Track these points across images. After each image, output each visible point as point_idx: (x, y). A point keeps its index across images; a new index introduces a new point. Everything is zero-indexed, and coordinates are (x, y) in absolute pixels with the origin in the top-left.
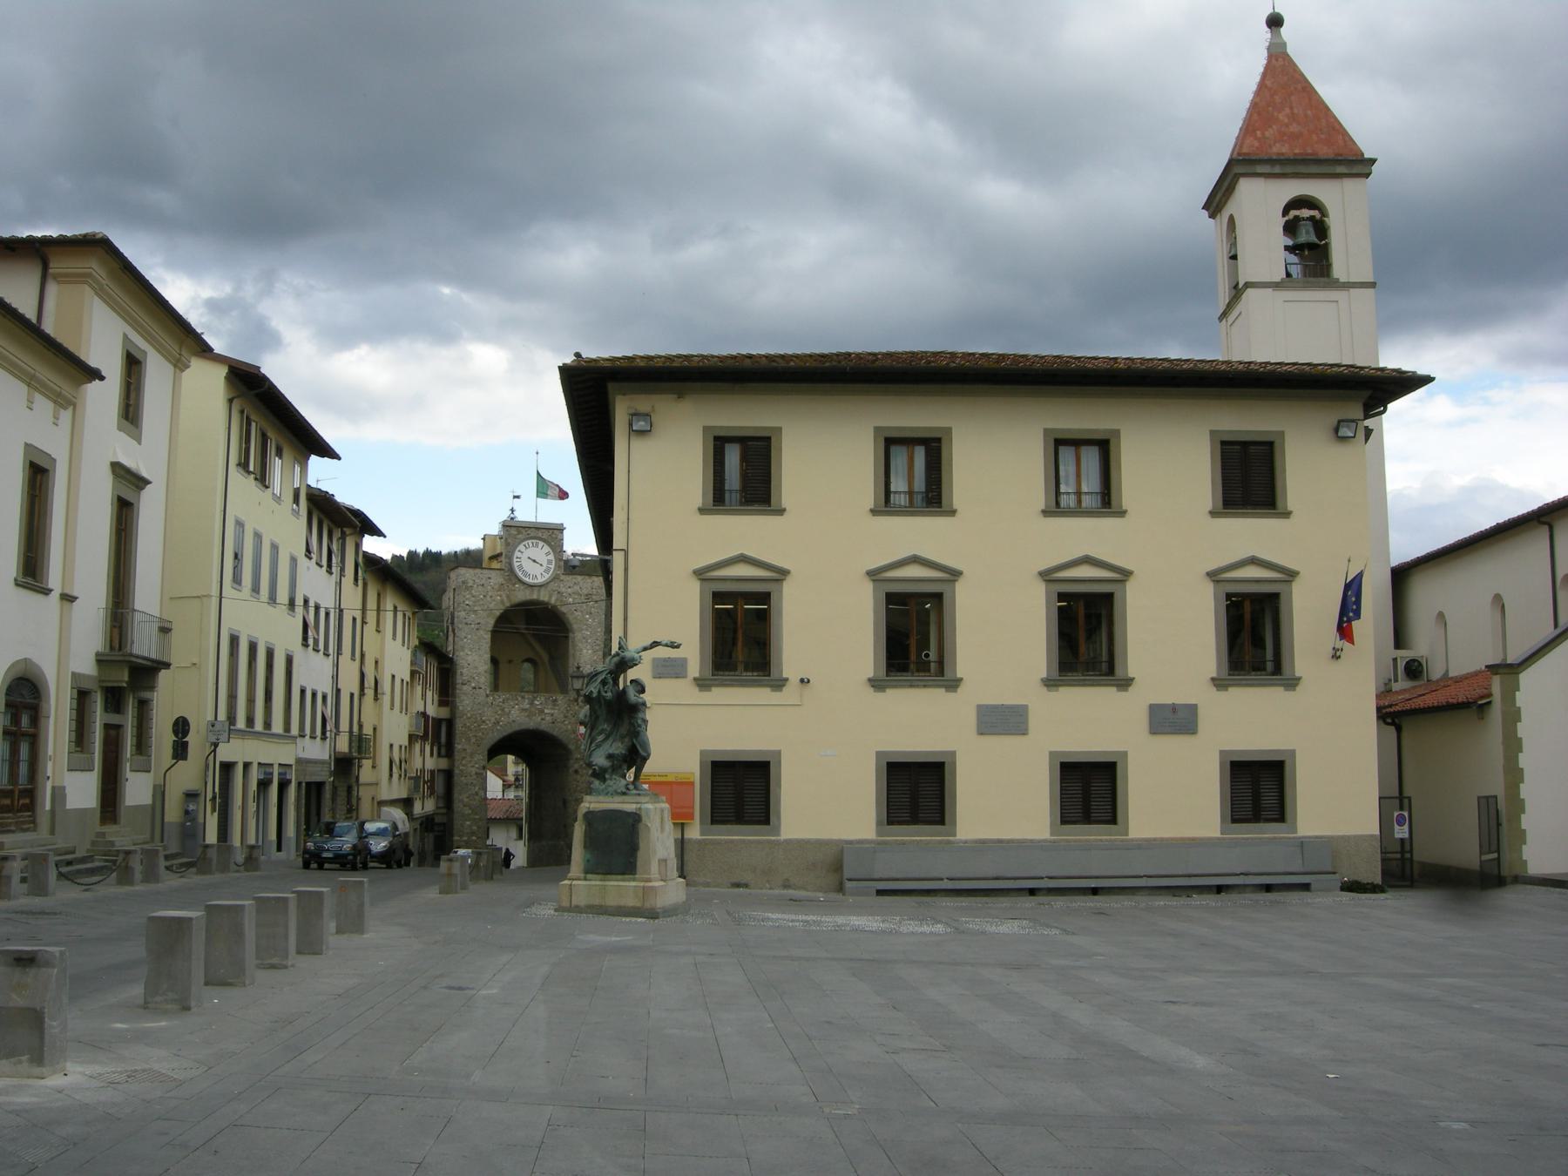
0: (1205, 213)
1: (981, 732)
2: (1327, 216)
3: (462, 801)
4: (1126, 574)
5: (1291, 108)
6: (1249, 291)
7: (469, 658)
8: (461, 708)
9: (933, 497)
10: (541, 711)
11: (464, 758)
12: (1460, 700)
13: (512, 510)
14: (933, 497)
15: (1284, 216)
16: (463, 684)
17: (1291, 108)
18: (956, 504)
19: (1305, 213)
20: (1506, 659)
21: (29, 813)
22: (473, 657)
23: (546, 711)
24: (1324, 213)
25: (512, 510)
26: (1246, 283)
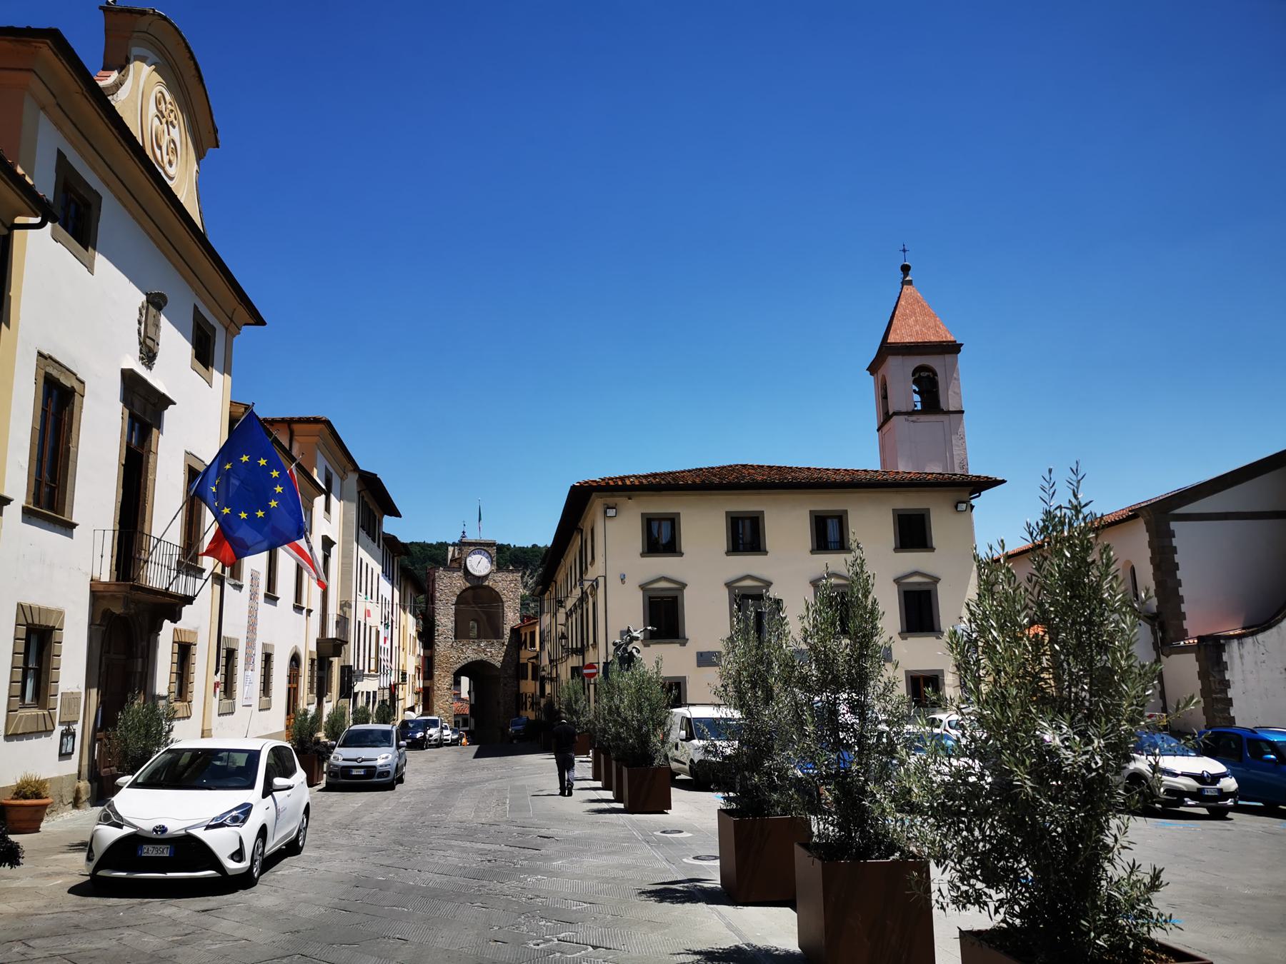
0: (868, 372)
1: (697, 653)
2: (937, 376)
3: (439, 706)
4: (684, 585)
5: (916, 318)
6: (895, 417)
7: (443, 621)
8: (21, 910)
9: (672, 548)
10: (484, 650)
11: (439, 680)
12: (496, 589)
13: (464, 532)
14: (672, 548)
15: (913, 376)
16: (438, 636)
17: (916, 318)
18: (683, 549)
19: (924, 374)
20: (1239, 643)
21: (740, 522)
22: (445, 620)
23: (488, 650)
24: (935, 374)
25: (464, 532)
26: (894, 413)
